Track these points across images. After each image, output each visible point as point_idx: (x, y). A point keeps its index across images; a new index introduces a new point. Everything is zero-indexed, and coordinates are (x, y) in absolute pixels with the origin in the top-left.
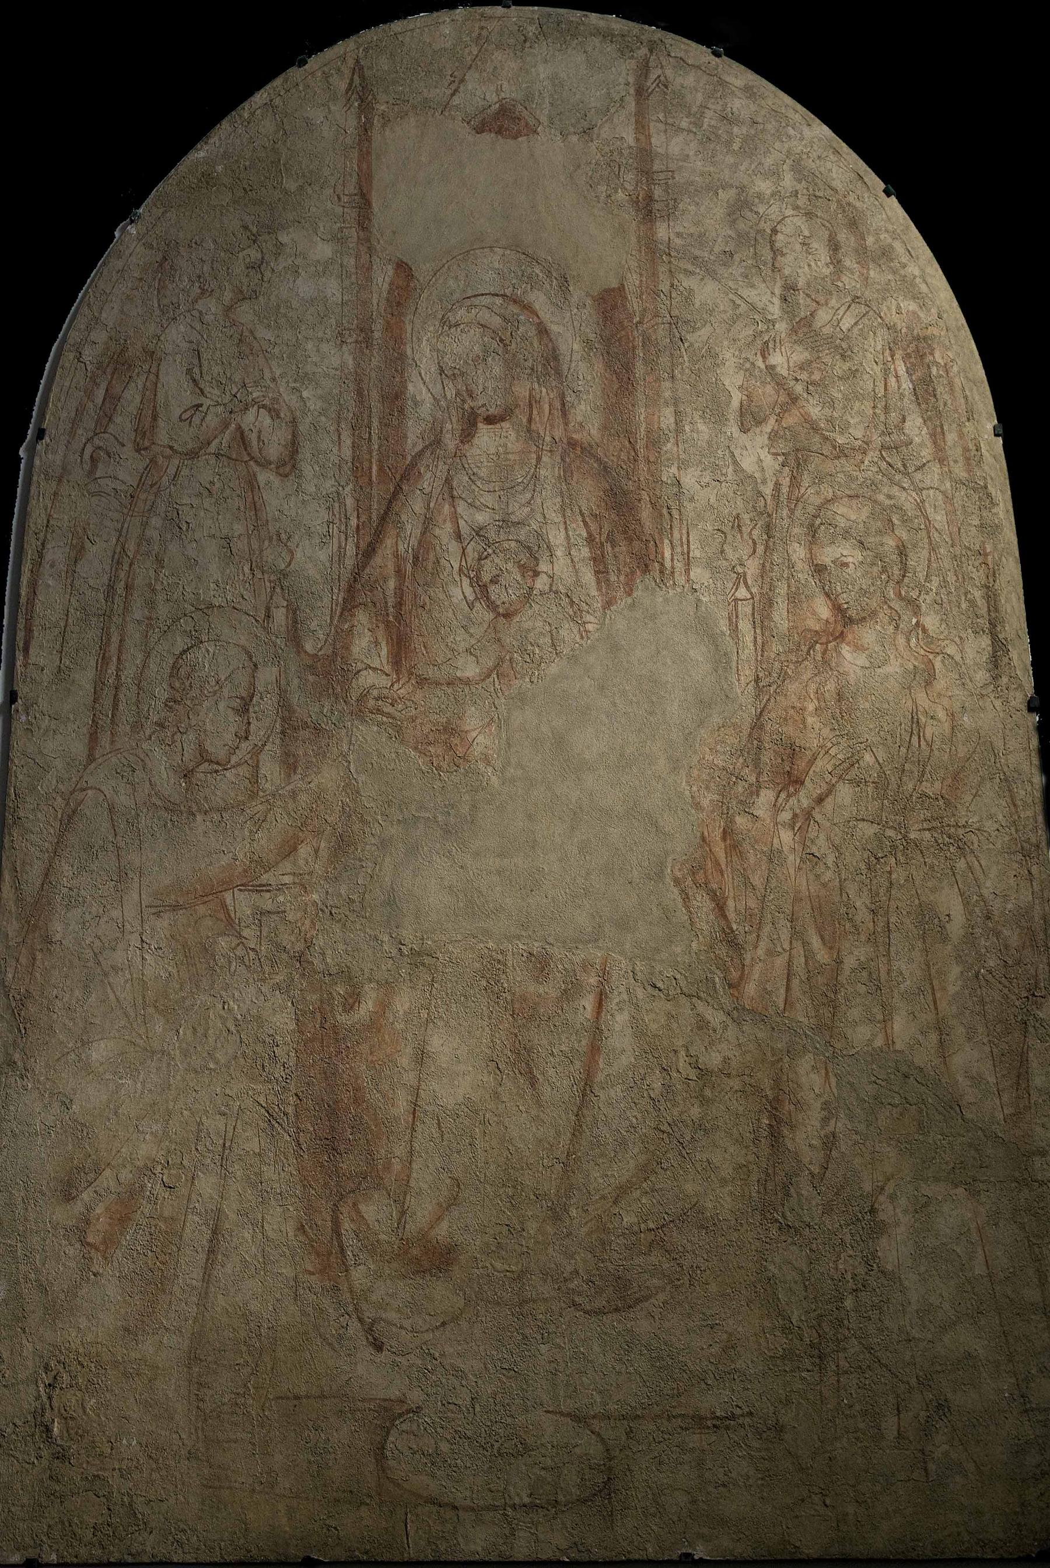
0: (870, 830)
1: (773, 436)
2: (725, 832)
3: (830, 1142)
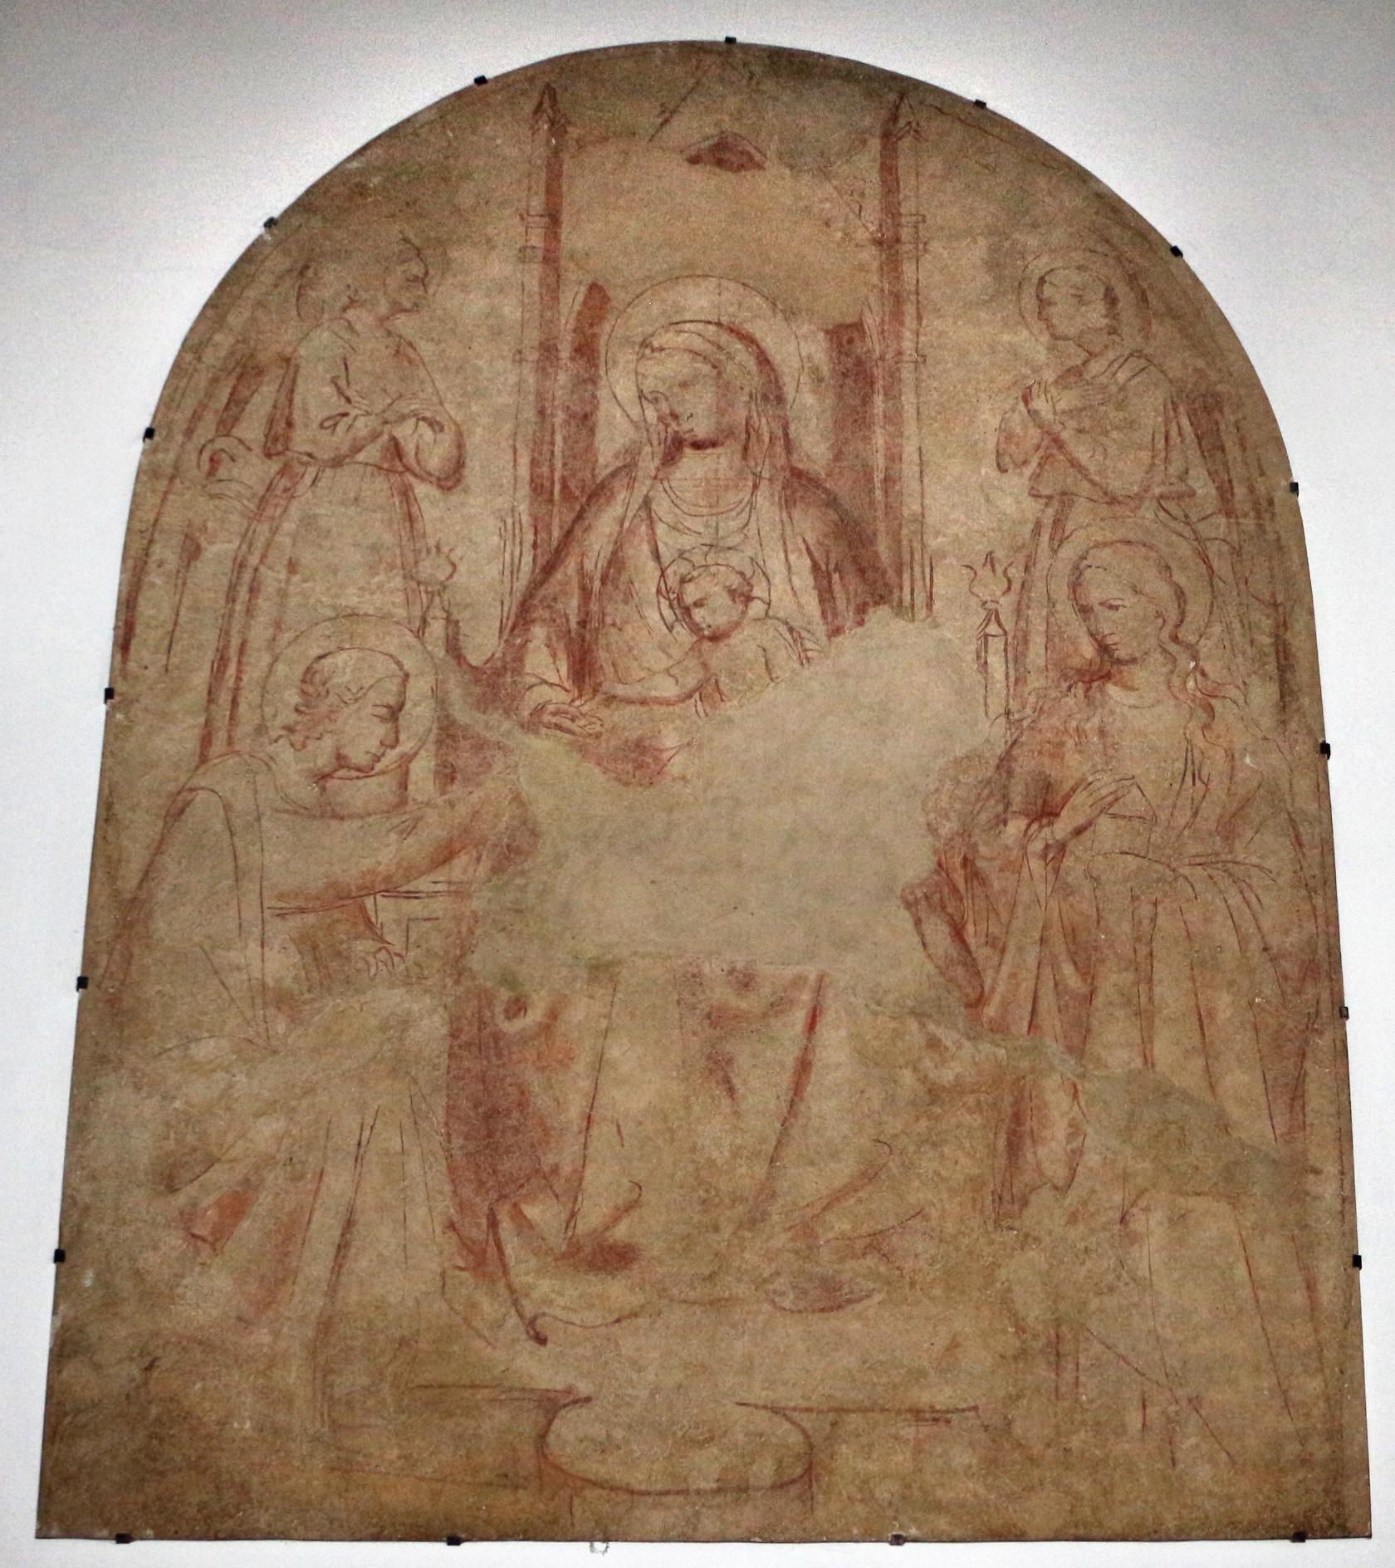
0: (1132, 863)
1: (1036, 477)
2: (965, 859)
3: (1074, 1159)
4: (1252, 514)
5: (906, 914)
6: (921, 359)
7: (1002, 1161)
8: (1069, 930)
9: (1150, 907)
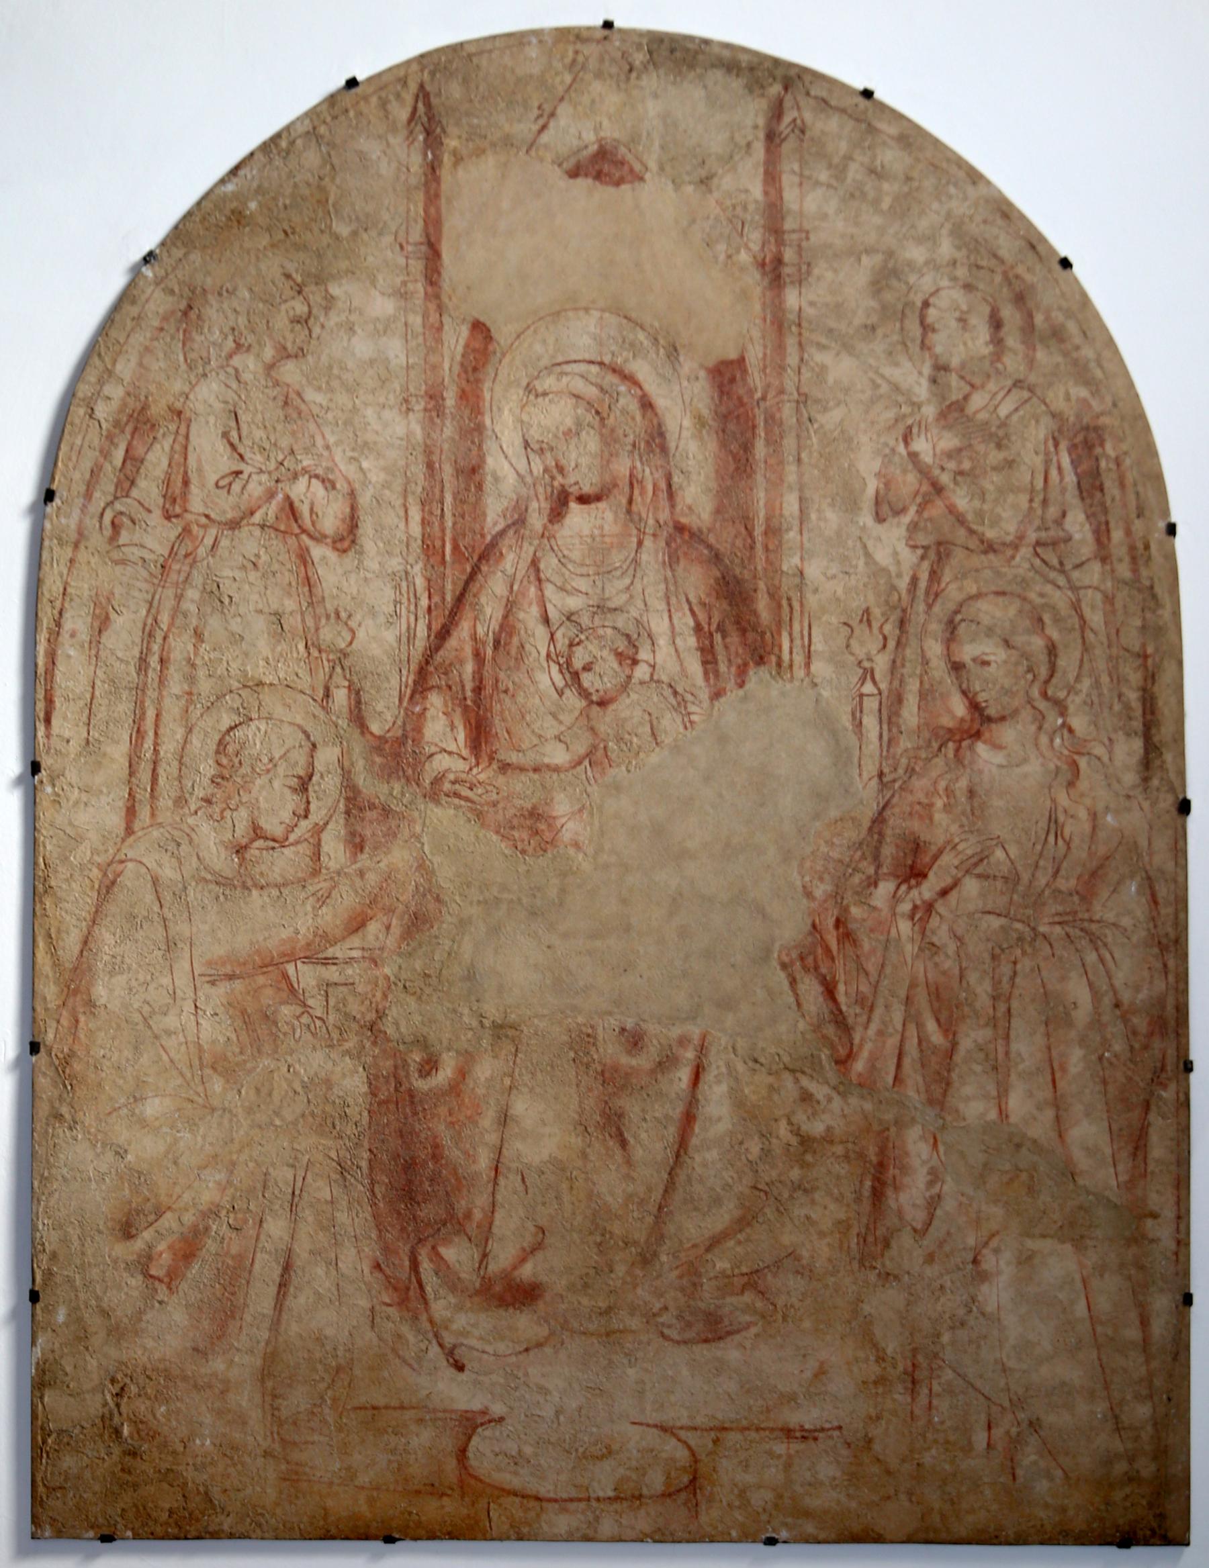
0: (996, 922)
1: (913, 527)
3: (933, 1203)
4: (1127, 559)
5: (782, 975)
7: (866, 1206)
8: (933, 989)
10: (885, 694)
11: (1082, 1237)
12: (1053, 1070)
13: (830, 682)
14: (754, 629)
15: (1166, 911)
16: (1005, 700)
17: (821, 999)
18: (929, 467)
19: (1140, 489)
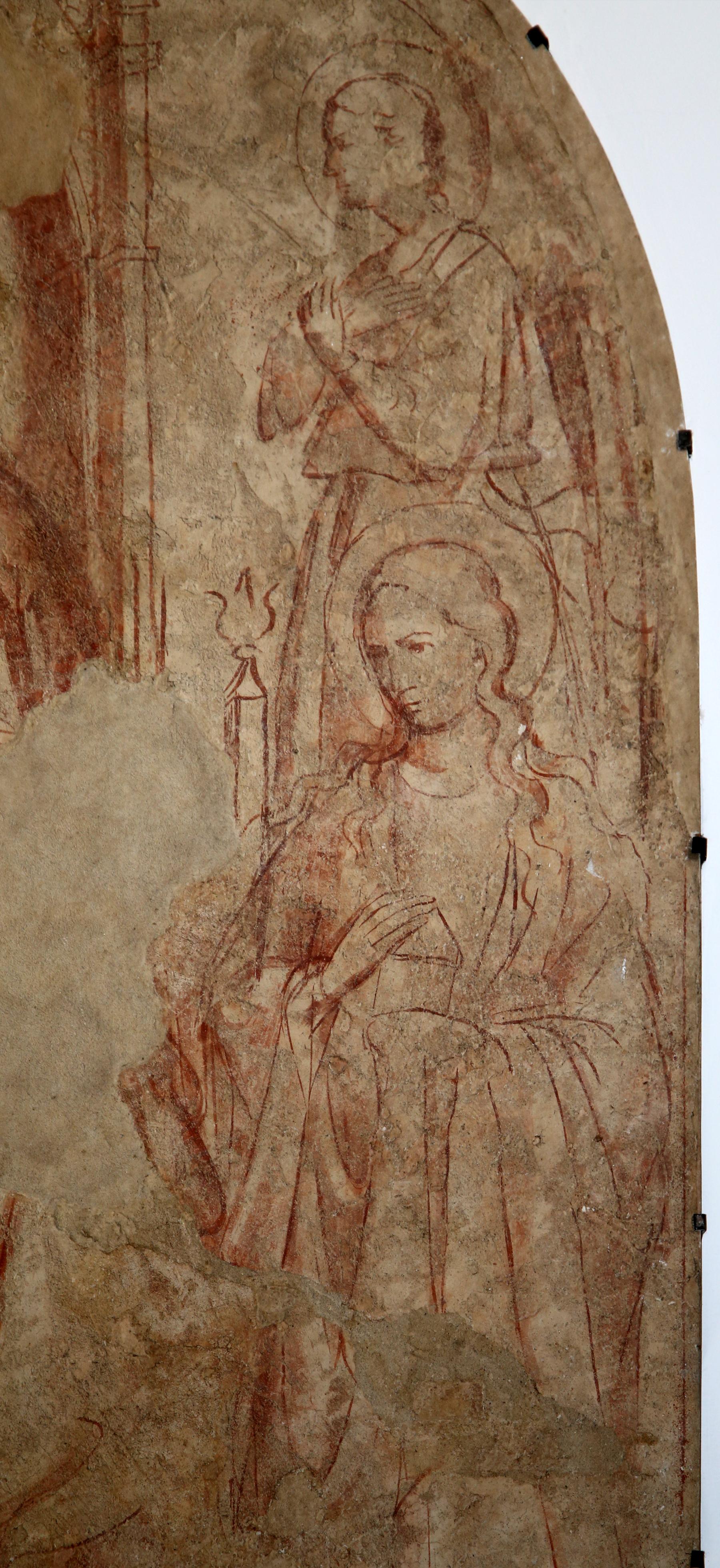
0: (428, 1023)
1: (314, 446)
2: (204, 1027)
3: (338, 1430)
4: (619, 486)
5: (125, 1108)
6: (153, 255)
7: (244, 1440)
8: (339, 1122)
9: (449, 1085)
10: (272, 695)
11: (547, 1474)
12: (509, 1235)
13: (193, 678)
14: (85, 605)
15: (670, 999)
16: (444, 700)
17: (180, 1142)
18: (337, 356)
19: (640, 382)
